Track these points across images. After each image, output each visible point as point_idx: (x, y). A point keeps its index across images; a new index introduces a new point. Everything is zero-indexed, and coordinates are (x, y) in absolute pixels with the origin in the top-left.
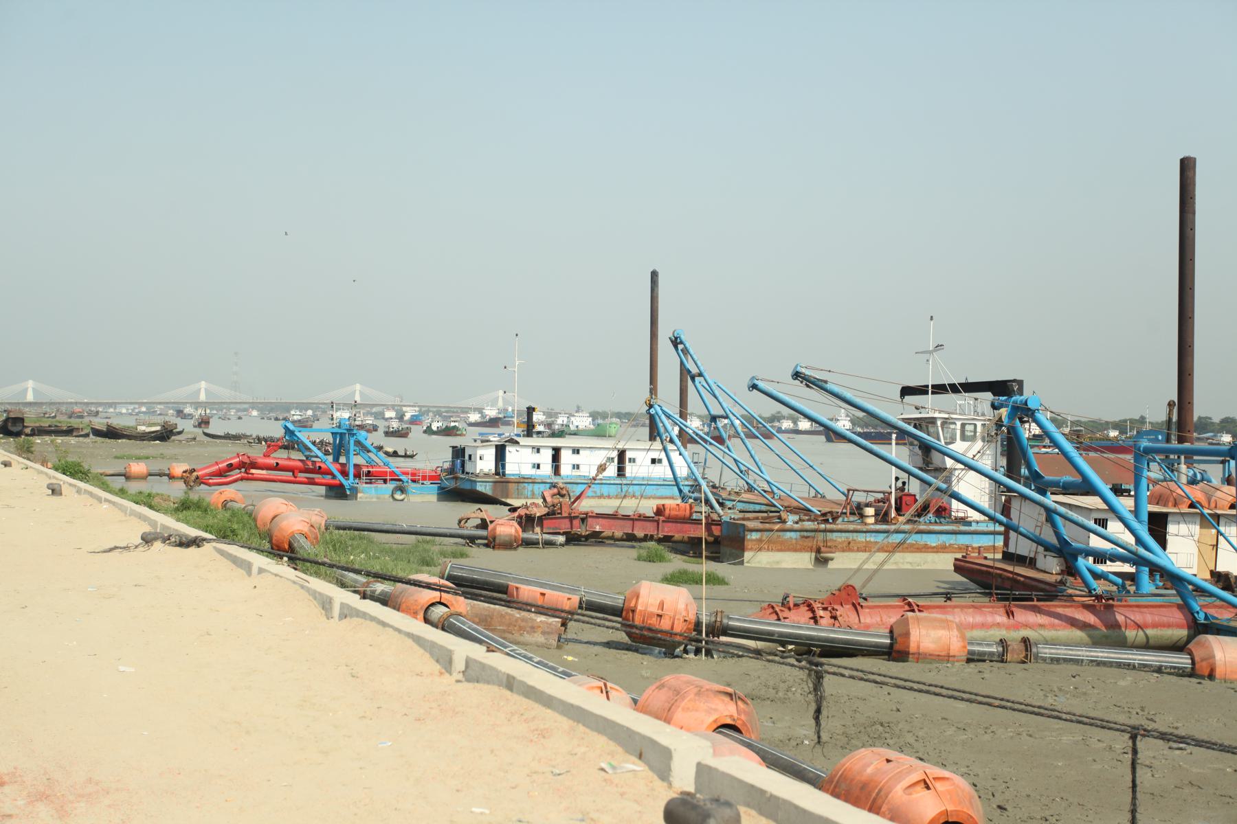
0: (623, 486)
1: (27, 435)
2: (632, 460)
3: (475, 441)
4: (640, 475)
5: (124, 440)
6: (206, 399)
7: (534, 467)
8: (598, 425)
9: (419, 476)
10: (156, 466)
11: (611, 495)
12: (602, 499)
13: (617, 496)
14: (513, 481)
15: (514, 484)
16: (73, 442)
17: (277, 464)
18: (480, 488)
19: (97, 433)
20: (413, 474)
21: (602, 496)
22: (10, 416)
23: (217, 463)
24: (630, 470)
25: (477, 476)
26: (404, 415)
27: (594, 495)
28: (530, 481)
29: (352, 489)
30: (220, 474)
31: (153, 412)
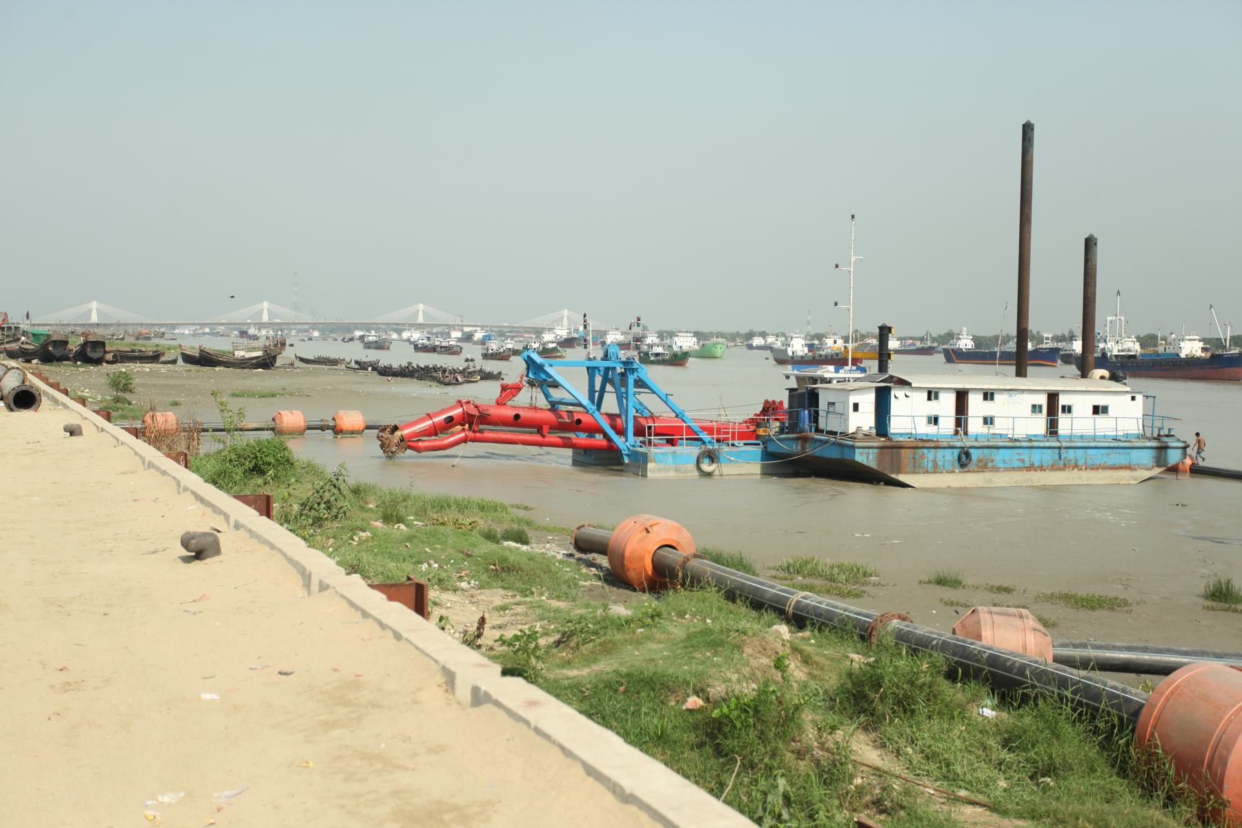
0: (1063, 451)
1: (108, 362)
2: (1067, 409)
3: (788, 377)
4: (1077, 432)
5: (222, 368)
6: (98, 320)
7: (929, 422)
8: (703, 345)
9: (728, 433)
10: (322, 414)
11: (1045, 464)
12: (1032, 472)
13: (1053, 465)
14: (908, 446)
15: (908, 450)
16: (163, 371)
17: (517, 417)
18: (861, 457)
19: (188, 359)
21: (1031, 468)
23: (429, 416)
25: (853, 437)
27: (1021, 465)
28: (932, 445)
29: (634, 455)
30: (434, 431)
31: (217, 332)
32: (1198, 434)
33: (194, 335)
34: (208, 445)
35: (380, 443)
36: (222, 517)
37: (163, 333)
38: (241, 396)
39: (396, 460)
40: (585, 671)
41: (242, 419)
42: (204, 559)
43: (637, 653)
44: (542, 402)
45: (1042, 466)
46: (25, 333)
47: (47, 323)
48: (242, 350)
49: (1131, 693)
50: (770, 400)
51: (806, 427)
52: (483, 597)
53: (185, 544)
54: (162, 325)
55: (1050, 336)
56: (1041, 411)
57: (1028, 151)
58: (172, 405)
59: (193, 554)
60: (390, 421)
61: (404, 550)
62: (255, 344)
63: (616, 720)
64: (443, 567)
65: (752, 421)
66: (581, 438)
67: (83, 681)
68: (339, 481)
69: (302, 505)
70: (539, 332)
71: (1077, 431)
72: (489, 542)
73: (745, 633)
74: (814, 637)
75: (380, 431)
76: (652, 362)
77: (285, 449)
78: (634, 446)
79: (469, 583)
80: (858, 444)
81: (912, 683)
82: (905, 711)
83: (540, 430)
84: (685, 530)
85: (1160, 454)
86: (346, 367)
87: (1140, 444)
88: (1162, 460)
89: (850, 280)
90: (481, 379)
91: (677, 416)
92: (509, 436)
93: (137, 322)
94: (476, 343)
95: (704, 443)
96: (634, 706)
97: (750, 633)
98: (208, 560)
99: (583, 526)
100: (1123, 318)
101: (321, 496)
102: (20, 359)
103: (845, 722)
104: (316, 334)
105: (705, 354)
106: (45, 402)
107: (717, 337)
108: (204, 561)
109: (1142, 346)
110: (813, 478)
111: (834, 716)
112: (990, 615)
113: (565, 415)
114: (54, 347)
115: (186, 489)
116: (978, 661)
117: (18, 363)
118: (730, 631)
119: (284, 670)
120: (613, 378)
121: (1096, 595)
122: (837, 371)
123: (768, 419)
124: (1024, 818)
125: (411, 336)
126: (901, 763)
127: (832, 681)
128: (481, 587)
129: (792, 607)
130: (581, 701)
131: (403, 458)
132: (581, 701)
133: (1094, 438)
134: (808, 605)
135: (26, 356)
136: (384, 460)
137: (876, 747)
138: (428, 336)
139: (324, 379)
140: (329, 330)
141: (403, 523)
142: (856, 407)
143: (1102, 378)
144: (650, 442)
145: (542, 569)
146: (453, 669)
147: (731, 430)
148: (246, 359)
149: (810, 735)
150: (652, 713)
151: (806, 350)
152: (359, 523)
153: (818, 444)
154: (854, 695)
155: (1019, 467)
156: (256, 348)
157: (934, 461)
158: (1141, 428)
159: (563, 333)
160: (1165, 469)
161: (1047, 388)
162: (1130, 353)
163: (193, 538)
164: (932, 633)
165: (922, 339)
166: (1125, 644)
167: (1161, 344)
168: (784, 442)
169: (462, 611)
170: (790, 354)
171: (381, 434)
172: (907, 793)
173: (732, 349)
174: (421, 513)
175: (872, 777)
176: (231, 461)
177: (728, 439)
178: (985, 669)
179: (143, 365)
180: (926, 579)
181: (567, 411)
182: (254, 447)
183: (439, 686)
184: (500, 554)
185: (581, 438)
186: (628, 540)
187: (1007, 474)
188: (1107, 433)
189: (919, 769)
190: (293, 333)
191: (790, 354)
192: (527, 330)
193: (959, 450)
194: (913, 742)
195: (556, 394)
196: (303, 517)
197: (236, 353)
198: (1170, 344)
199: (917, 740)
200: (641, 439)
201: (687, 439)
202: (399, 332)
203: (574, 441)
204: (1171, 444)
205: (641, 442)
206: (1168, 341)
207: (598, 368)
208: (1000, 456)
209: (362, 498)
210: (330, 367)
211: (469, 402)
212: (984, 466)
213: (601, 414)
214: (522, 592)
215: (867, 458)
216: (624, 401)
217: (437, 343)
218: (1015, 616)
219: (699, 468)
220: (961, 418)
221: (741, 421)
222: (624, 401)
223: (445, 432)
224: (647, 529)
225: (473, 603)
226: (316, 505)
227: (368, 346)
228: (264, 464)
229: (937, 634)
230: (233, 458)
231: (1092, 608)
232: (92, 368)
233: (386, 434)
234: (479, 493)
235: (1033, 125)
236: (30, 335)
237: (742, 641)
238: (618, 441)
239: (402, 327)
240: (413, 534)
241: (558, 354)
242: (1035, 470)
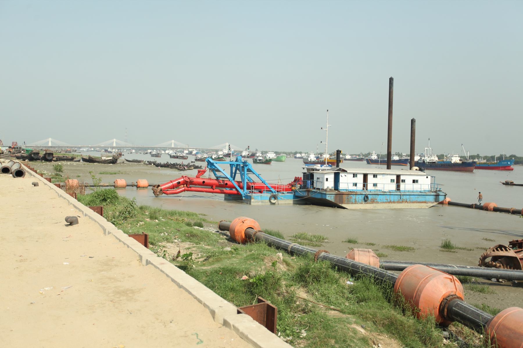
0: (402, 196)
1: (54, 161)
3: (304, 169)
4: (407, 189)
5: (97, 163)
6: (116, 145)
9: (281, 189)
12: (391, 204)
13: (398, 201)
16: (75, 164)
17: (204, 182)
19: (84, 160)
20: (278, 188)
21: (390, 202)
22: (47, 153)
23: (171, 182)
24: (402, 186)
25: (326, 190)
26: (192, 152)
27: (386, 201)
28: (354, 193)
30: (173, 187)
32: (480, 193)
33: (87, 151)
34: (88, 191)
35: (153, 191)
36: (81, 212)
37: (76, 150)
38: (103, 174)
39: (159, 198)
40: (209, 267)
41: (100, 182)
42: (73, 225)
43: (228, 262)
44: (213, 177)
45: (394, 202)
46: (23, 150)
47: (32, 146)
48: (105, 157)
49: (395, 275)
50: (297, 177)
51: (309, 187)
52: (182, 245)
53: (67, 220)
54: (76, 147)
55: (405, 154)
56: (394, 182)
57: (391, 87)
58: (77, 177)
59: (69, 223)
60: (157, 183)
61: (155, 228)
62: (110, 154)
63: (217, 283)
64: (169, 235)
65: (290, 184)
66: (227, 190)
67: (27, 259)
68: (133, 204)
69: (120, 212)
70: (217, 151)
71: (407, 189)
72: (187, 226)
73: (265, 255)
74: (296, 258)
75: (153, 187)
76: (258, 163)
77: (115, 192)
78: (246, 193)
79: (178, 240)
80: (327, 193)
81: (319, 271)
82: (317, 281)
83: (212, 188)
84: (257, 222)
85: (437, 197)
86: (144, 163)
87: (429, 194)
88: (437, 199)
89: (326, 133)
90: (194, 168)
91: (262, 182)
92: (201, 189)
93: (66, 146)
94: (193, 155)
95: (272, 192)
96: (224, 279)
97: (267, 255)
98: (74, 225)
99: (222, 221)
100: (431, 148)
101: (127, 209)
102: (21, 159)
103: (297, 285)
104: (134, 151)
105: (278, 160)
106: (27, 174)
107: (283, 154)
108: (73, 226)
109: (439, 159)
110: (311, 205)
111: (293, 283)
112: (358, 251)
113: (221, 182)
114: (34, 155)
115: (71, 204)
116: (348, 266)
117: (20, 161)
118: (260, 254)
119: (91, 256)
120: (239, 168)
121: (404, 246)
122: (321, 167)
123: (296, 184)
124: (350, 314)
125: (169, 152)
126: (313, 298)
127: (295, 270)
128: (182, 242)
129: (290, 248)
130: (206, 277)
131: (161, 197)
132: (206, 277)
133: (413, 192)
134: (295, 248)
135: (23, 158)
136: (155, 197)
137: (306, 293)
138: (175, 152)
139: (136, 167)
140: (139, 149)
141: (157, 219)
142: (327, 180)
143: (416, 170)
144: (252, 192)
145: (205, 236)
146: (142, 255)
147: (282, 188)
148: (106, 160)
149: (283, 289)
150: (230, 281)
151: (315, 159)
152: (141, 219)
153: (313, 193)
154: (300, 275)
155: (386, 202)
156: (109, 156)
157: (355, 199)
158: (430, 188)
159: (226, 151)
160: (438, 203)
161: (396, 173)
162: (433, 161)
163: (69, 218)
164: (335, 257)
165: (359, 155)
166: (404, 261)
167: (445, 158)
168: (302, 192)
169: (174, 249)
170: (309, 160)
171: (153, 188)
172: (314, 307)
173: (289, 158)
174: (164, 216)
175: (302, 302)
176: (95, 197)
177: (281, 191)
178: (350, 268)
179: (67, 162)
180: (345, 241)
181: (222, 180)
182: (104, 192)
183: (138, 260)
184: (190, 230)
185: (227, 190)
186: (236, 226)
187: (381, 204)
188: (418, 190)
189: (319, 299)
190: (125, 150)
191: (309, 160)
192: (213, 150)
193: (364, 195)
194: (318, 291)
195: (218, 174)
196: (120, 217)
197: (102, 158)
198: (448, 158)
199: (320, 290)
200: (250, 191)
201: (266, 191)
202: (165, 151)
203: (225, 191)
204: (440, 194)
205: (249, 192)
206: (448, 157)
207: (234, 164)
208: (379, 198)
209: (143, 211)
210: (138, 163)
211: (186, 177)
212: (373, 201)
213: (234, 181)
214: (196, 243)
215: (331, 198)
216: (243, 176)
217: (178, 155)
218: (367, 252)
219: (270, 202)
220: (365, 184)
221: (286, 184)
222: (243, 176)
223: (178, 187)
224: (243, 222)
225: (178, 247)
226: (125, 213)
227: (153, 156)
228: (107, 198)
229: (336, 257)
230: (96, 195)
231: (401, 251)
232: (48, 163)
233: (155, 188)
234: (191, 210)
235: (393, 78)
236: (25, 151)
237: (264, 257)
238: (241, 191)
239: (166, 149)
240: (159, 223)
241: (224, 159)
242: (392, 203)
